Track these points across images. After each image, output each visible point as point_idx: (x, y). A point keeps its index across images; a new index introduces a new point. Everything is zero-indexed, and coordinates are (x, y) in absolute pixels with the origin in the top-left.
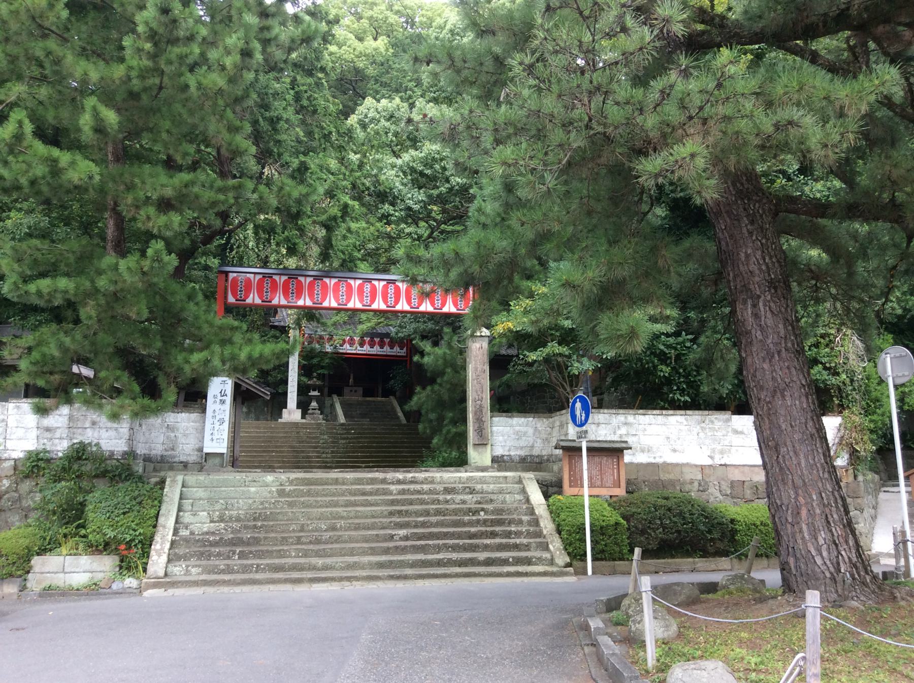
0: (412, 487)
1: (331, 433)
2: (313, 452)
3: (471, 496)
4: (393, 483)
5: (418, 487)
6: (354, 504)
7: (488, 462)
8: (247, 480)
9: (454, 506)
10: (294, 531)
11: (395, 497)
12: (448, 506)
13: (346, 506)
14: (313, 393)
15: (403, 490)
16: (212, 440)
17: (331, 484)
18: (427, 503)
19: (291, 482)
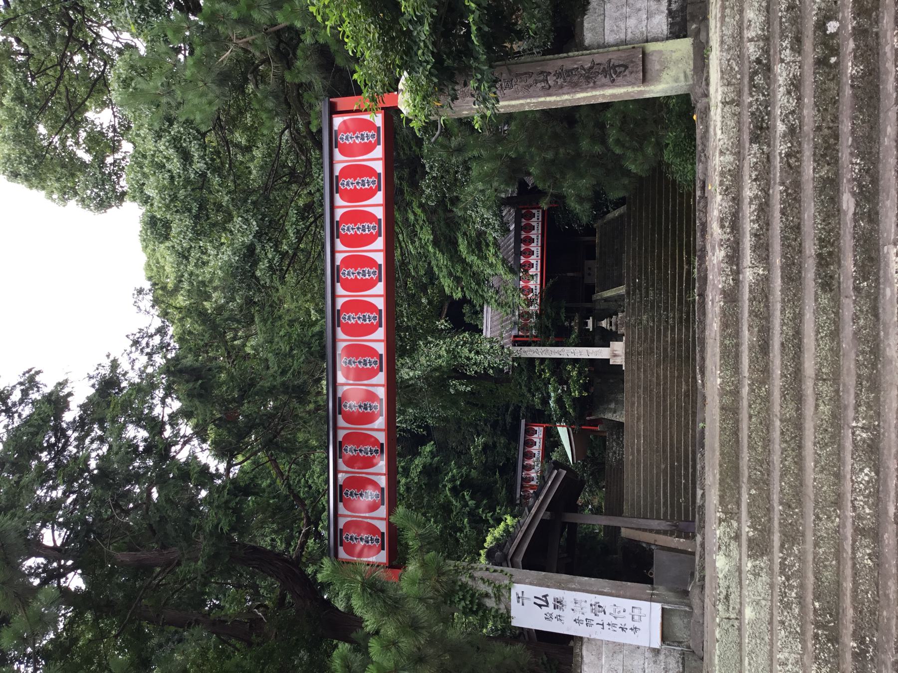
0: (749, 226)
1: (640, 310)
2: (665, 336)
3: (778, 68)
4: (737, 273)
5: (749, 211)
6: (796, 375)
7: (684, 45)
8: (722, 614)
9: (809, 112)
10: (876, 556)
11: (778, 273)
12: (808, 127)
13: (799, 399)
14: (590, 326)
15: (755, 249)
16: (634, 629)
17: (737, 422)
18: (797, 185)
19: (731, 515)
